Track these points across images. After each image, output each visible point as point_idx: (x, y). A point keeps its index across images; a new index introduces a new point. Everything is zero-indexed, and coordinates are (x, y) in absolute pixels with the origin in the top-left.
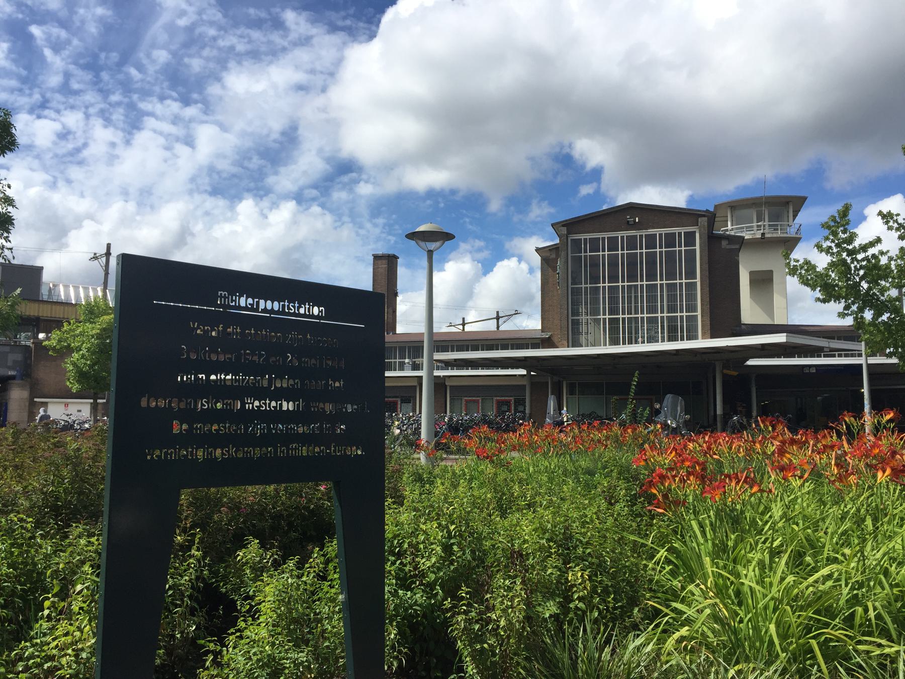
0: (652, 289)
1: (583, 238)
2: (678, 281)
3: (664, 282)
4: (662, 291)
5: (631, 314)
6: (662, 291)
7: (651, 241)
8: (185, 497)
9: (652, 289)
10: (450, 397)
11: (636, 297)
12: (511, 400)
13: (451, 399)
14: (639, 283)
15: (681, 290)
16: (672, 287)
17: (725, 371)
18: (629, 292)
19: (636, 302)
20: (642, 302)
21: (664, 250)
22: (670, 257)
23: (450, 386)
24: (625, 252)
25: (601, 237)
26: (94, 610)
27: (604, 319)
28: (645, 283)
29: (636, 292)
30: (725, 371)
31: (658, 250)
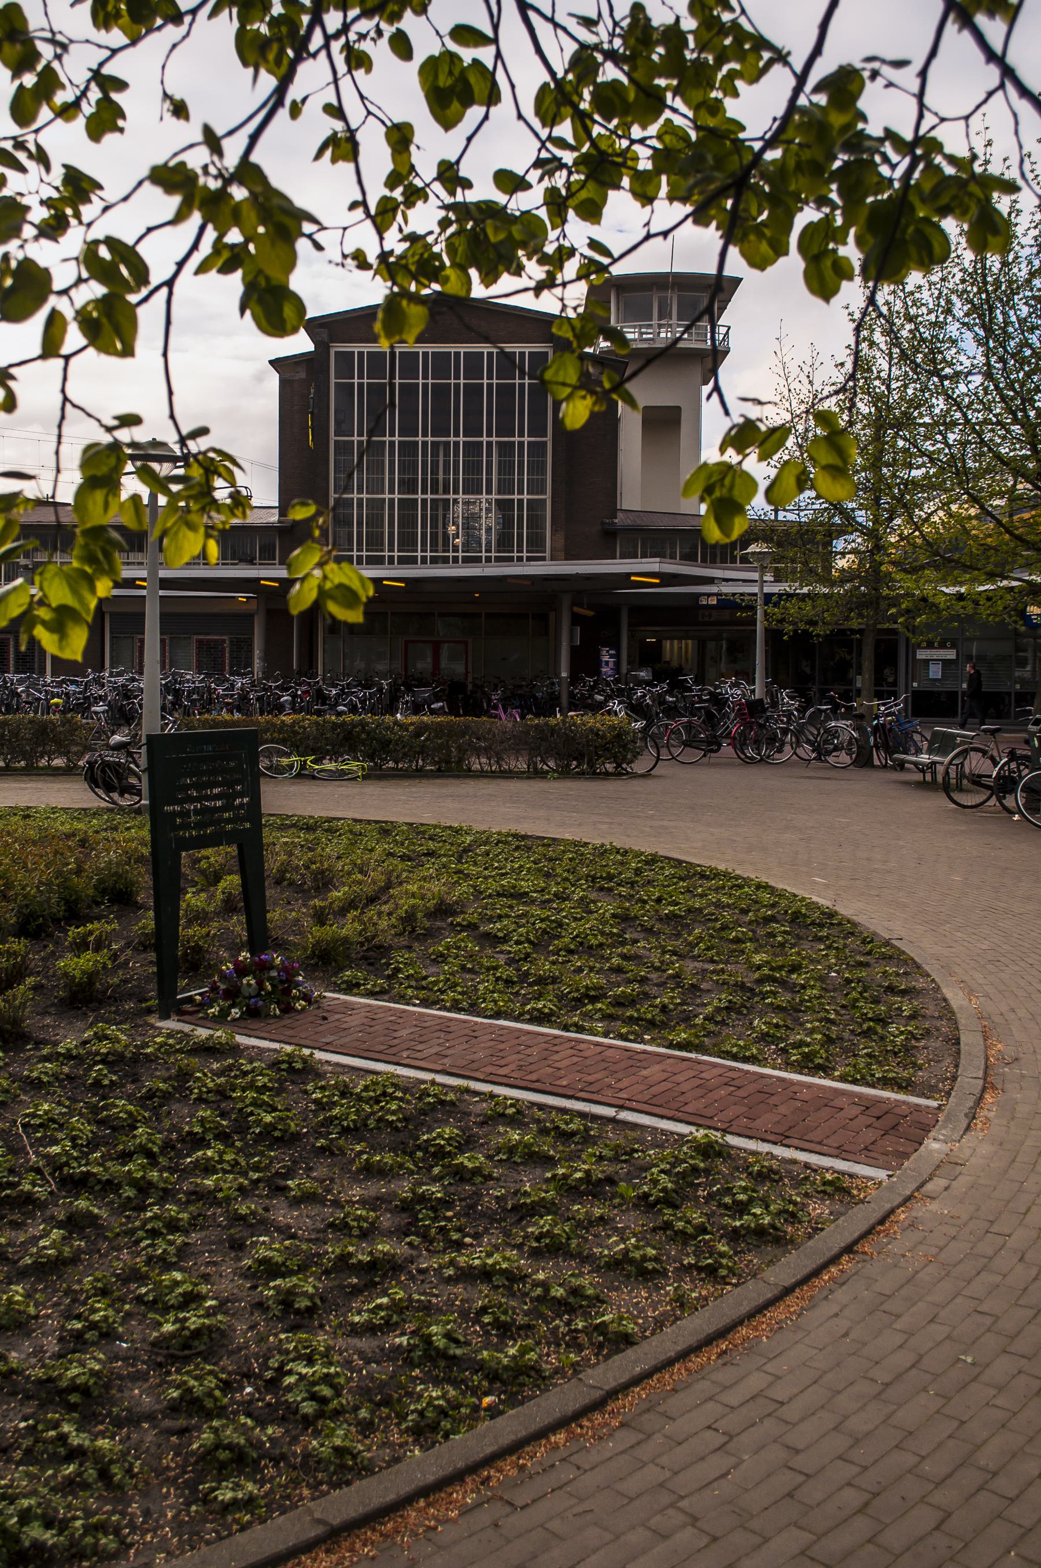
0: (474, 449)
1: (356, 350)
2: (517, 439)
3: (494, 439)
4: (489, 454)
5: (437, 493)
6: (489, 454)
7: (507, 363)
8: (184, 854)
9: (474, 449)
10: (111, 633)
11: (446, 464)
12: (224, 641)
13: (112, 638)
14: (452, 439)
15: (521, 455)
16: (506, 449)
17: (576, 609)
18: (435, 454)
19: (446, 471)
20: (456, 472)
21: (430, 381)
22: (507, 392)
23: (112, 614)
24: (365, 381)
25: (453, 350)
26: (56, 1149)
27: (392, 501)
28: (396, 439)
29: (447, 454)
30: (576, 609)
31: (485, 381)
